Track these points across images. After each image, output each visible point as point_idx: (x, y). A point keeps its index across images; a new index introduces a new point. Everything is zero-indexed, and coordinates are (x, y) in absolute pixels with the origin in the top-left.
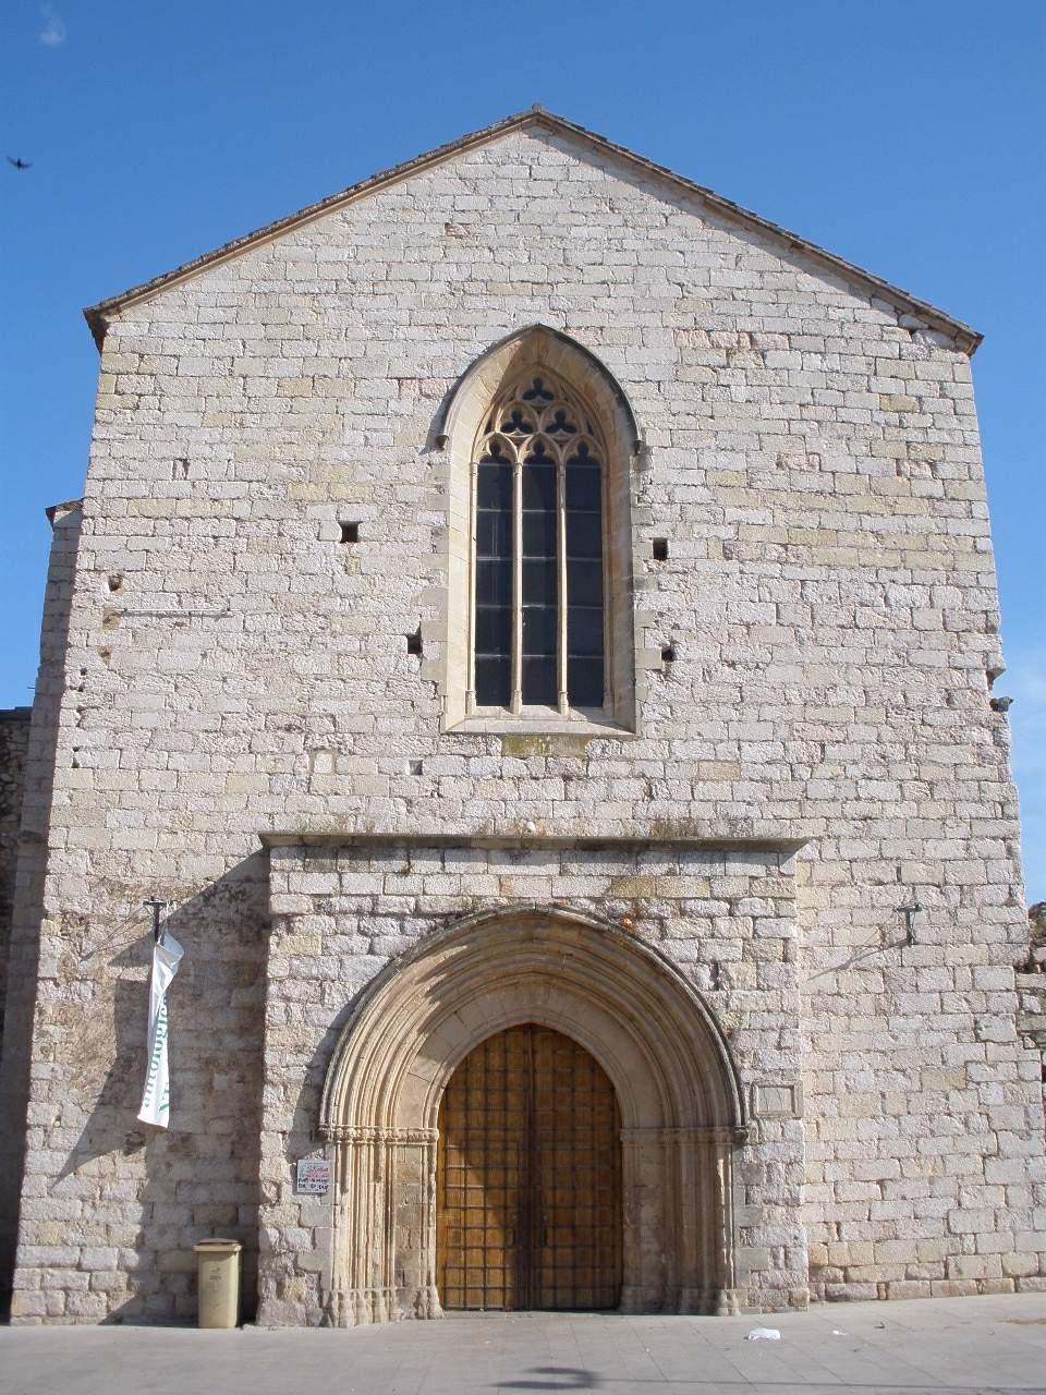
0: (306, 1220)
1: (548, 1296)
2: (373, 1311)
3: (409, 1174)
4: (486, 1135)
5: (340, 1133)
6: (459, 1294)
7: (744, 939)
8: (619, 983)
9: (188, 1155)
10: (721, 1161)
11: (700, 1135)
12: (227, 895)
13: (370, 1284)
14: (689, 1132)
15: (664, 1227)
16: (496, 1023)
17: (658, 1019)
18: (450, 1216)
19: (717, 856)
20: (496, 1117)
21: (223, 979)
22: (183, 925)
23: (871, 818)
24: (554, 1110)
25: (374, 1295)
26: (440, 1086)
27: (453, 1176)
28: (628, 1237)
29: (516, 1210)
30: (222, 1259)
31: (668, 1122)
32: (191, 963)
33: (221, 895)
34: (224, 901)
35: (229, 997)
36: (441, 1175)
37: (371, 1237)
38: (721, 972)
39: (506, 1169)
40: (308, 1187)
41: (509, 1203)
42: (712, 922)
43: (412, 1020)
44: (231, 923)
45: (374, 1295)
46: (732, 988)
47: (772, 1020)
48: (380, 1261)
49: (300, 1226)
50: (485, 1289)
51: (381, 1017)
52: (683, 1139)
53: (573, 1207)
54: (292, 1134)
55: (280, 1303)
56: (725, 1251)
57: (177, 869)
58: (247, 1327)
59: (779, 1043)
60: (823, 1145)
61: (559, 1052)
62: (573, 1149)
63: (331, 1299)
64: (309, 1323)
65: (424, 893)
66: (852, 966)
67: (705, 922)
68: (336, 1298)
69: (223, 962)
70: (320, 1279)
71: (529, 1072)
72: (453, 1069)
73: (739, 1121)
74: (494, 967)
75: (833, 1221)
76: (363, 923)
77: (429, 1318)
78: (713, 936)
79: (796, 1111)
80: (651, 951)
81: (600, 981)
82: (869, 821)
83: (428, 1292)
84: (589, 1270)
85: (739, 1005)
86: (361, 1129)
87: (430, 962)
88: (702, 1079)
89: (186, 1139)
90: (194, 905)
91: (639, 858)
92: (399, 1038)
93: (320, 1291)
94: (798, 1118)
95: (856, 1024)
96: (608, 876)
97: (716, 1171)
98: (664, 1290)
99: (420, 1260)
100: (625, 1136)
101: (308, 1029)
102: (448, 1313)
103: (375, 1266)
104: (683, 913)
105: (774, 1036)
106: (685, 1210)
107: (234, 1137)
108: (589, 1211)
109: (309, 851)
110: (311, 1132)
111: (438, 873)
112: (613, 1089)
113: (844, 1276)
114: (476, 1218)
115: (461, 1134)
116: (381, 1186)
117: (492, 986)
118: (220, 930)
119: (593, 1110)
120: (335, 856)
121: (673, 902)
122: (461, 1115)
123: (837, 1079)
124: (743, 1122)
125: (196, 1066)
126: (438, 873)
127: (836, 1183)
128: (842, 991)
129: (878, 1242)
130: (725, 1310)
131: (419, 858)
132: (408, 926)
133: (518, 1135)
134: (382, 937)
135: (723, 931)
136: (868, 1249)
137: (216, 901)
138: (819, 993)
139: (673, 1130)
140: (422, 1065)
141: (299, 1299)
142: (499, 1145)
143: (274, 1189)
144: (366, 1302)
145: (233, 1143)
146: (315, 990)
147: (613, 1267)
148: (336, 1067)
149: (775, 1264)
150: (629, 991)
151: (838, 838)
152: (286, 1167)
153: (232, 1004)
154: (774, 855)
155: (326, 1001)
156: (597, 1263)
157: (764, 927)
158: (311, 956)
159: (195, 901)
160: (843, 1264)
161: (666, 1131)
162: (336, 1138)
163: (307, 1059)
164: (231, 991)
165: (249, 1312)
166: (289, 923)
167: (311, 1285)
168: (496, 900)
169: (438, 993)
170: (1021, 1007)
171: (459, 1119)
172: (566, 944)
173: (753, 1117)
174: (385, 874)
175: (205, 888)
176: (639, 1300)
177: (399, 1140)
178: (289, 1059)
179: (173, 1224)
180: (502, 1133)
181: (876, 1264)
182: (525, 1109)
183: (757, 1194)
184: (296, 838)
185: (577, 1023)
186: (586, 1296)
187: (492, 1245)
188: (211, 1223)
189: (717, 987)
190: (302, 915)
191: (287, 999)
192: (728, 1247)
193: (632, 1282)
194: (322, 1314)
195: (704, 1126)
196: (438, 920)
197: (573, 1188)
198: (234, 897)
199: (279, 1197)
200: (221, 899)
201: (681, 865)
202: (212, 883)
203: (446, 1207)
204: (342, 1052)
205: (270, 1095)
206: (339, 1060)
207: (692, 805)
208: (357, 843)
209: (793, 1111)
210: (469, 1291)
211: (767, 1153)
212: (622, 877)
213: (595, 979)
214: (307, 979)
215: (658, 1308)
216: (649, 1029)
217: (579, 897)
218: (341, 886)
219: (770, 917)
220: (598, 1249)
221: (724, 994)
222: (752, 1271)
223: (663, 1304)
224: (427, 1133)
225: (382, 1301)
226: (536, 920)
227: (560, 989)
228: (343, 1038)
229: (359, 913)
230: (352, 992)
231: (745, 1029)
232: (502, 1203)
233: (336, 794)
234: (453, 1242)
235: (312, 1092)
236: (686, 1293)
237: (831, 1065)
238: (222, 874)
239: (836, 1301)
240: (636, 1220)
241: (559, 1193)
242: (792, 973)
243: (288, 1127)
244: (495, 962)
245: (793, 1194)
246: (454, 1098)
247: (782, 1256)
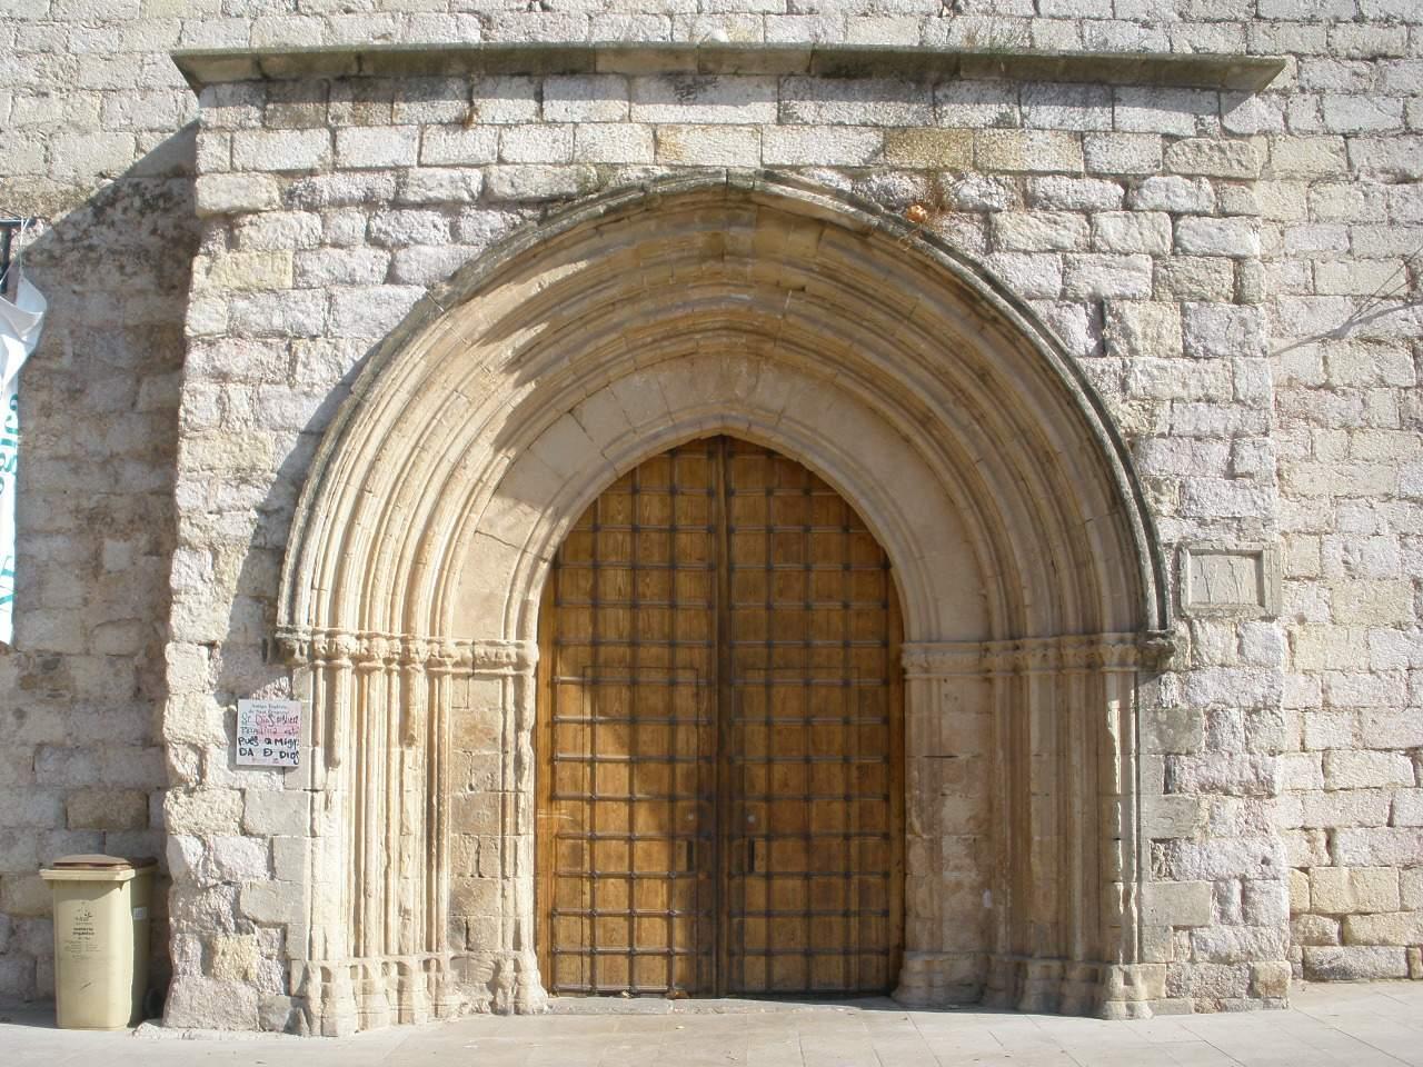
0: (256, 822)
1: (755, 970)
2: (400, 999)
3: (476, 731)
4: (634, 657)
5: (321, 643)
6: (578, 962)
7: (1155, 256)
8: (898, 344)
9: (55, 694)
10: (1115, 705)
11: (1070, 652)
12: (137, 202)
13: (394, 948)
14: (1046, 646)
15: (988, 836)
16: (653, 432)
17: (981, 419)
18: (563, 814)
19: (1096, 92)
20: (654, 620)
21: (125, 359)
22: (54, 260)
23: (1385, 57)
24: (769, 607)
25: (402, 969)
26: (539, 558)
27: (568, 735)
28: (917, 856)
29: (693, 803)
30: (93, 897)
31: (999, 627)
32: (66, 332)
33: (126, 202)
34: (132, 214)
35: (137, 393)
36: (544, 734)
37: (394, 855)
38: (1109, 319)
39: (673, 724)
40: (259, 755)
41: (680, 791)
42: (1089, 220)
43: (479, 420)
44: (142, 253)
45: (402, 969)
46: (1133, 351)
47: (1212, 419)
48: (415, 904)
49: (245, 832)
50: (631, 955)
51: (407, 408)
52: (1032, 662)
53: (807, 799)
54: (228, 648)
55: (207, 984)
56: (1121, 887)
57: (46, 161)
58: (147, 1028)
59: (1231, 465)
60: (1302, 679)
61: (779, 493)
62: (807, 684)
63: (306, 977)
64: (265, 1026)
65: (501, 161)
66: (1352, 333)
67: (1075, 220)
68: (317, 978)
69: (126, 327)
70: (285, 938)
71: (720, 530)
72: (565, 522)
73: (1155, 620)
74: (647, 314)
75: (1321, 825)
76: (376, 224)
77: (518, 1012)
78: (1091, 248)
79: (1268, 603)
80: (968, 271)
81: (860, 342)
82: (1381, 62)
83: (516, 961)
84: (837, 921)
85: (1152, 384)
86: (370, 638)
87: (510, 296)
88: (1072, 533)
89: (52, 664)
90: (75, 225)
91: (939, 94)
92: (453, 455)
93: (286, 961)
94: (1269, 619)
95: (1364, 444)
96: (876, 125)
97: (1103, 725)
98: (988, 960)
99: (499, 899)
100: (913, 658)
101: (262, 435)
102: (556, 1000)
103: (404, 912)
104: (1030, 201)
105: (1218, 453)
106: (1035, 803)
107: (140, 660)
108: (838, 807)
109: (275, 89)
110: (265, 641)
111: (529, 122)
112: (886, 565)
113: (1341, 933)
114: (613, 819)
115: (584, 654)
116: (416, 755)
117: (644, 356)
118: (122, 268)
119: (846, 606)
120: (325, 98)
121: (1009, 179)
122: (585, 618)
123: (1328, 549)
124: (1163, 624)
125: (71, 525)
126: (529, 122)
127: (1326, 751)
128: (1335, 381)
129: (1407, 867)
130: (1119, 1007)
131: (493, 94)
132: (467, 226)
133: (699, 656)
134: (413, 252)
135: (1113, 238)
136: (1388, 882)
137: (116, 214)
138: (1291, 383)
139: (1010, 644)
140: (503, 513)
141: (245, 977)
142: (658, 677)
143: (193, 758)
144: (382, 983)
145: (138, 670)
146: (279, 357)
147: (886, 913)
148: (312, 508)
149: (1223, 914)
150: (919, 359)
151: (1320, 92)
152: (215, 714)
153: (141, 405)
154: (1210, 96)
155: (298, 378)
156: (854, 907)
157: (1196, 234)
158: (273, 291)
159: (78, 217)
160: (1340, 909)
161: (995, 646)
162: (313, 655)
163: (256, 495)
164: (139, 381)
165: (152, 1001)
166: (231, 230)
167: (267, 950)
168: (646, 170)
169: (531, 367)
171: (579, 625)
172: (794, 265)
173: (1182, 617)
174: (423, 127)
175: (97, 190)
176: (938, 980)
177: (456, 664)
178: (225, 496)
179: (29, 825)
180: (665, 652)
181: (1404, 909)
182: (710, 607)
183: (1187, 774)
184: (248, 63)
185: (814, 431)
186: (831, 970)
187: (646, 870)
188: (100, 822)
189: (1103, 349)
190: (256, 212)
191: (222, 377)
192: (1127, 881)
193: (925, 946)
194: (289, 1009)
195: (1077, 633)
196: (528, 213)
197: (807, 760)
198: (148, 206)
199: (202, 772)
200: (125, 210)
201: (1025, 109)
202: (109, 181)
203: (553, 798)
204: (324, 476)
205: (186, 570)
206: (317, 493)
207: (1034, 25)
208: (368, 70)
209: (1262, 604)
210: (600, 959)
211: (1209, 688)
212: (904, 129)
213: (850, 337)
214: (263, 336)
215: (978, 995)
216: (962, 438)
217: (818, 166)
218: (335, 152)
219: (1206, 214)
220: (855, 880)
221: (1117, 363)
222: (1176, 928)
223: (988, 989)
224: (513, 651)
225: (418, 979)
226: (735, 203)
227: (779, 365)
228: (326, 448)
229: (369, 203)
230: (350, 357)
231: (1162, 435)
232: (665, 789)
233: (348, 11)
234: (568, 866)
235: (267, 561)
236: (1035, 969)
237: (1315, 521)
238: (129, 165)
239: (1324, 981)
240: (933, 824)
241: (779, 770)
242: (1252, 327)
243: (220, 636)
244: (649, 305)
245: (1262, 773)
246: (570, 577)
247: (1237, 898)
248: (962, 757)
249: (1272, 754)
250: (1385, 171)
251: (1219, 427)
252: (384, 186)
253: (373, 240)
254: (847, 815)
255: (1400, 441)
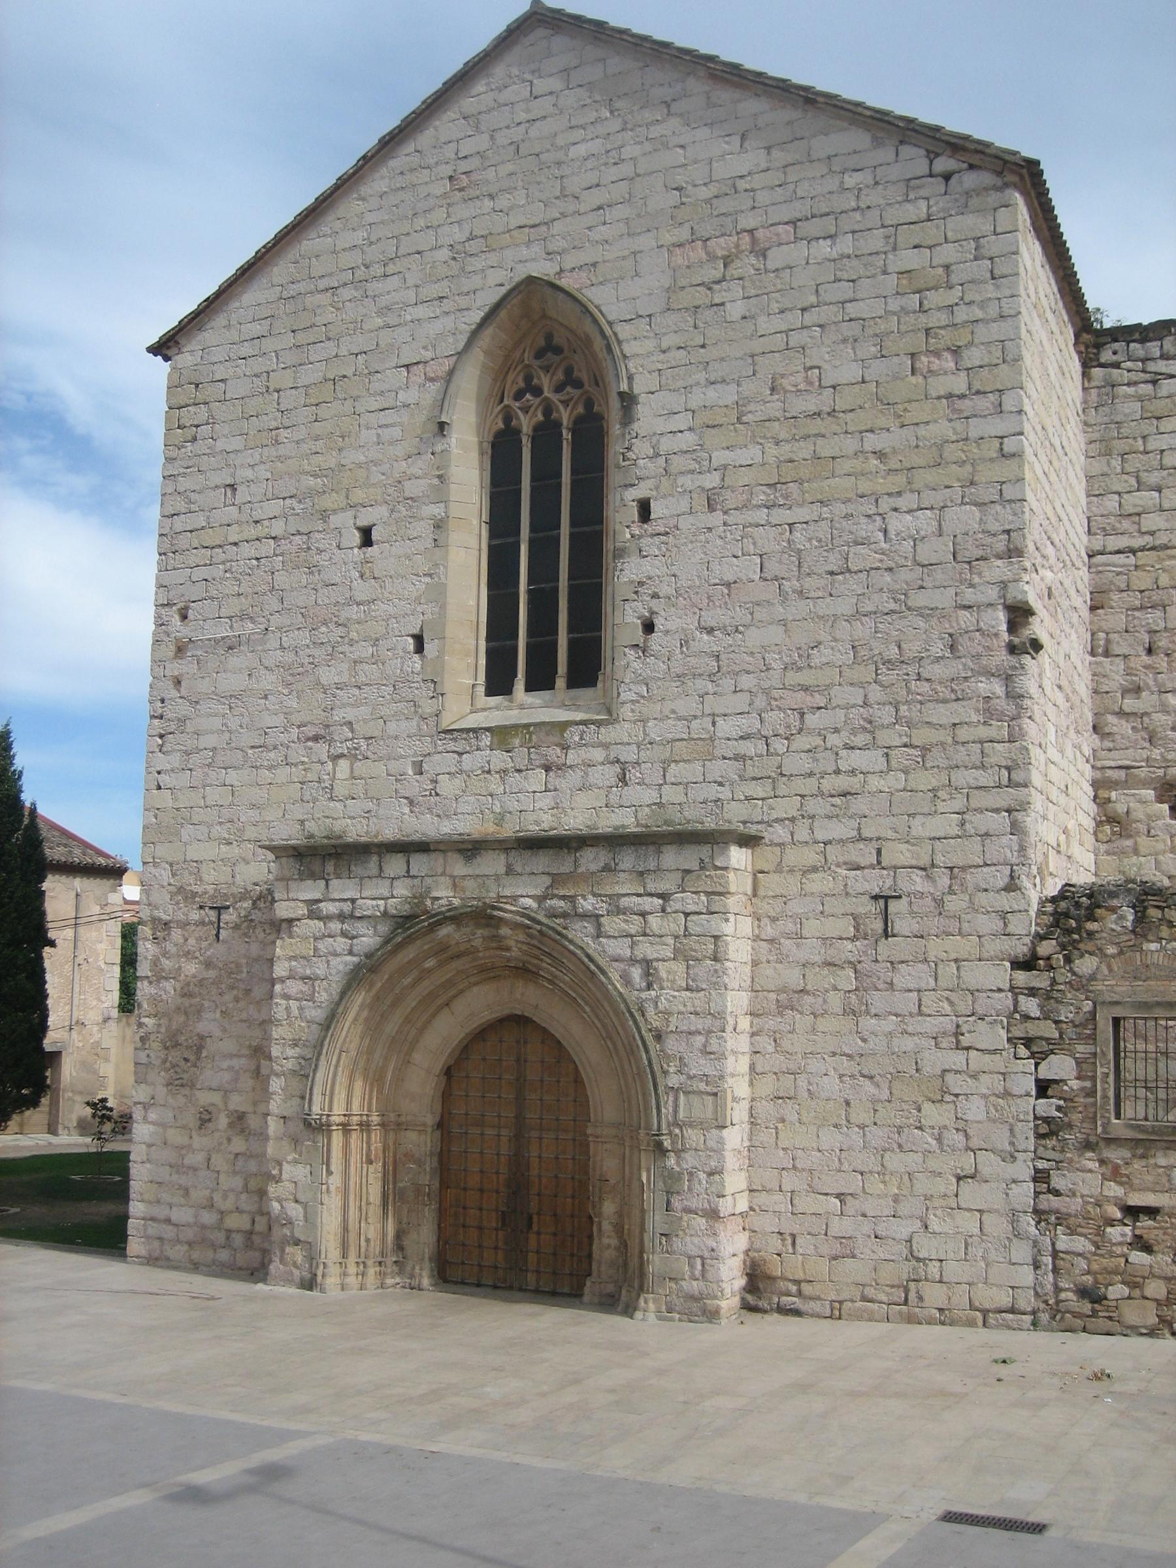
7: (676, 937)
9: (242, 1131)
13: (362, 1255)
63: (317, 1267)
78: (645, 935)
84: (568, 1258)
95: (823, 1024)
103: (368, 1241)
123: (799, 1083)
128: (809, 987)
151: (812, 817)
170: (1016, 1010)
183: (676, 1203)
190: (299, 920)
191: (287, 997)
248: (612, 1182)
249: (719, 1197)
250: (845, 863)
251: (700, 1027)
252: (347, 907)
253: (344, 934)
254: (573, 1204)
255: (843, 1022)
